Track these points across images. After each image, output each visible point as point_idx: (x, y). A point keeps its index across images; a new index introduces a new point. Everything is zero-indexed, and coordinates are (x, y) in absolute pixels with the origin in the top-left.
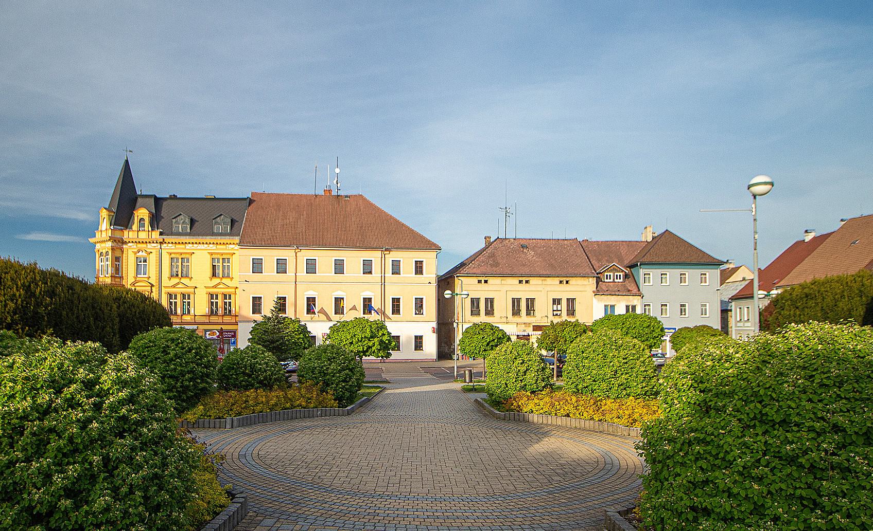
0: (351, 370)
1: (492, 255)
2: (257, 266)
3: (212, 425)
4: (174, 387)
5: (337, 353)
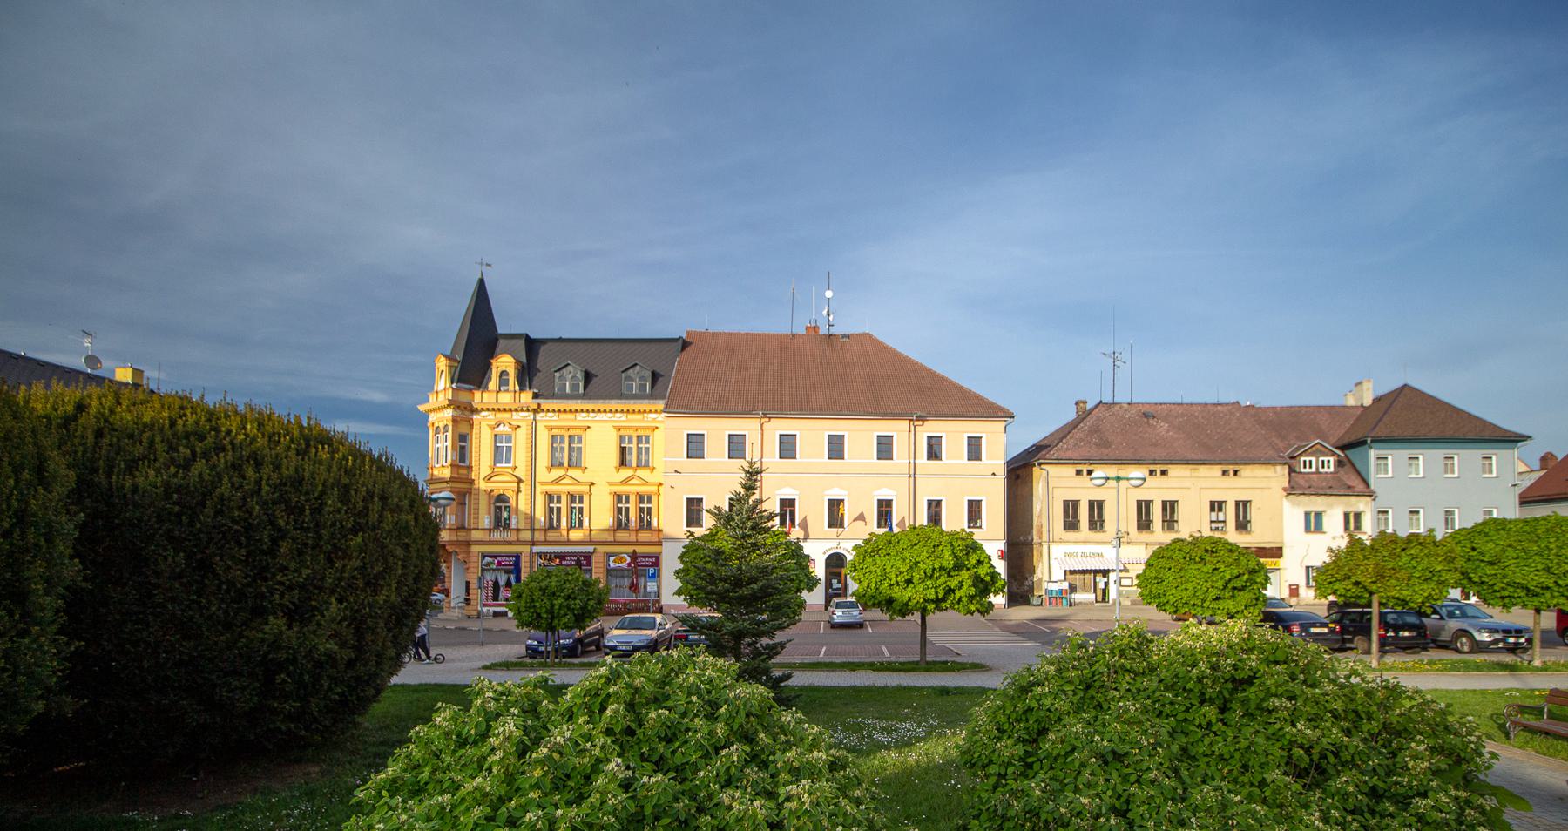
1: (1096, 430)
2: (695, 446)
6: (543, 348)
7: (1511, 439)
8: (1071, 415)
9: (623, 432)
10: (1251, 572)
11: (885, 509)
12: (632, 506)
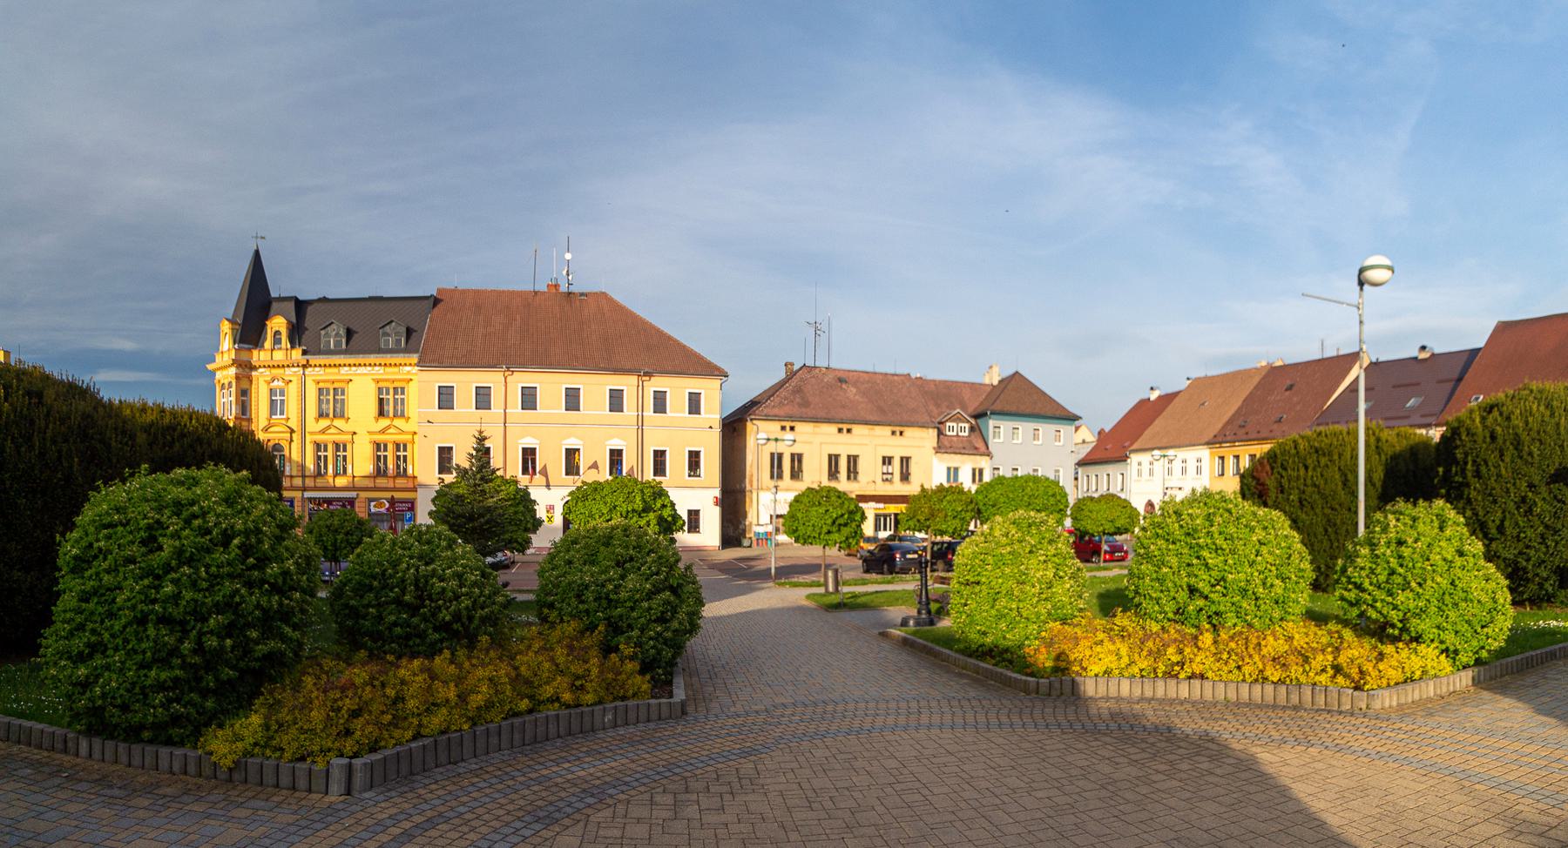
0: (674, 590)
1: (798, 390)
2: (446, 398)
3: (285, 780)
4: (174, 652)
5: (638, 547)
6: (310, 308)
7: (1071, 418)
8: (781, 375)
9: (381, 384)
10: (851, 513)
11: (616, 457)
12: (390, 454)
